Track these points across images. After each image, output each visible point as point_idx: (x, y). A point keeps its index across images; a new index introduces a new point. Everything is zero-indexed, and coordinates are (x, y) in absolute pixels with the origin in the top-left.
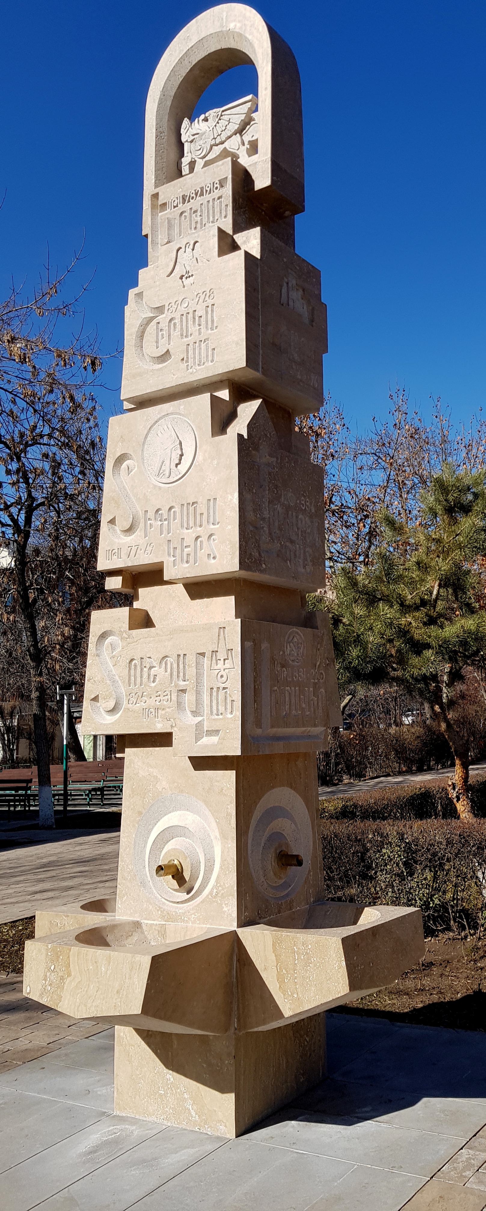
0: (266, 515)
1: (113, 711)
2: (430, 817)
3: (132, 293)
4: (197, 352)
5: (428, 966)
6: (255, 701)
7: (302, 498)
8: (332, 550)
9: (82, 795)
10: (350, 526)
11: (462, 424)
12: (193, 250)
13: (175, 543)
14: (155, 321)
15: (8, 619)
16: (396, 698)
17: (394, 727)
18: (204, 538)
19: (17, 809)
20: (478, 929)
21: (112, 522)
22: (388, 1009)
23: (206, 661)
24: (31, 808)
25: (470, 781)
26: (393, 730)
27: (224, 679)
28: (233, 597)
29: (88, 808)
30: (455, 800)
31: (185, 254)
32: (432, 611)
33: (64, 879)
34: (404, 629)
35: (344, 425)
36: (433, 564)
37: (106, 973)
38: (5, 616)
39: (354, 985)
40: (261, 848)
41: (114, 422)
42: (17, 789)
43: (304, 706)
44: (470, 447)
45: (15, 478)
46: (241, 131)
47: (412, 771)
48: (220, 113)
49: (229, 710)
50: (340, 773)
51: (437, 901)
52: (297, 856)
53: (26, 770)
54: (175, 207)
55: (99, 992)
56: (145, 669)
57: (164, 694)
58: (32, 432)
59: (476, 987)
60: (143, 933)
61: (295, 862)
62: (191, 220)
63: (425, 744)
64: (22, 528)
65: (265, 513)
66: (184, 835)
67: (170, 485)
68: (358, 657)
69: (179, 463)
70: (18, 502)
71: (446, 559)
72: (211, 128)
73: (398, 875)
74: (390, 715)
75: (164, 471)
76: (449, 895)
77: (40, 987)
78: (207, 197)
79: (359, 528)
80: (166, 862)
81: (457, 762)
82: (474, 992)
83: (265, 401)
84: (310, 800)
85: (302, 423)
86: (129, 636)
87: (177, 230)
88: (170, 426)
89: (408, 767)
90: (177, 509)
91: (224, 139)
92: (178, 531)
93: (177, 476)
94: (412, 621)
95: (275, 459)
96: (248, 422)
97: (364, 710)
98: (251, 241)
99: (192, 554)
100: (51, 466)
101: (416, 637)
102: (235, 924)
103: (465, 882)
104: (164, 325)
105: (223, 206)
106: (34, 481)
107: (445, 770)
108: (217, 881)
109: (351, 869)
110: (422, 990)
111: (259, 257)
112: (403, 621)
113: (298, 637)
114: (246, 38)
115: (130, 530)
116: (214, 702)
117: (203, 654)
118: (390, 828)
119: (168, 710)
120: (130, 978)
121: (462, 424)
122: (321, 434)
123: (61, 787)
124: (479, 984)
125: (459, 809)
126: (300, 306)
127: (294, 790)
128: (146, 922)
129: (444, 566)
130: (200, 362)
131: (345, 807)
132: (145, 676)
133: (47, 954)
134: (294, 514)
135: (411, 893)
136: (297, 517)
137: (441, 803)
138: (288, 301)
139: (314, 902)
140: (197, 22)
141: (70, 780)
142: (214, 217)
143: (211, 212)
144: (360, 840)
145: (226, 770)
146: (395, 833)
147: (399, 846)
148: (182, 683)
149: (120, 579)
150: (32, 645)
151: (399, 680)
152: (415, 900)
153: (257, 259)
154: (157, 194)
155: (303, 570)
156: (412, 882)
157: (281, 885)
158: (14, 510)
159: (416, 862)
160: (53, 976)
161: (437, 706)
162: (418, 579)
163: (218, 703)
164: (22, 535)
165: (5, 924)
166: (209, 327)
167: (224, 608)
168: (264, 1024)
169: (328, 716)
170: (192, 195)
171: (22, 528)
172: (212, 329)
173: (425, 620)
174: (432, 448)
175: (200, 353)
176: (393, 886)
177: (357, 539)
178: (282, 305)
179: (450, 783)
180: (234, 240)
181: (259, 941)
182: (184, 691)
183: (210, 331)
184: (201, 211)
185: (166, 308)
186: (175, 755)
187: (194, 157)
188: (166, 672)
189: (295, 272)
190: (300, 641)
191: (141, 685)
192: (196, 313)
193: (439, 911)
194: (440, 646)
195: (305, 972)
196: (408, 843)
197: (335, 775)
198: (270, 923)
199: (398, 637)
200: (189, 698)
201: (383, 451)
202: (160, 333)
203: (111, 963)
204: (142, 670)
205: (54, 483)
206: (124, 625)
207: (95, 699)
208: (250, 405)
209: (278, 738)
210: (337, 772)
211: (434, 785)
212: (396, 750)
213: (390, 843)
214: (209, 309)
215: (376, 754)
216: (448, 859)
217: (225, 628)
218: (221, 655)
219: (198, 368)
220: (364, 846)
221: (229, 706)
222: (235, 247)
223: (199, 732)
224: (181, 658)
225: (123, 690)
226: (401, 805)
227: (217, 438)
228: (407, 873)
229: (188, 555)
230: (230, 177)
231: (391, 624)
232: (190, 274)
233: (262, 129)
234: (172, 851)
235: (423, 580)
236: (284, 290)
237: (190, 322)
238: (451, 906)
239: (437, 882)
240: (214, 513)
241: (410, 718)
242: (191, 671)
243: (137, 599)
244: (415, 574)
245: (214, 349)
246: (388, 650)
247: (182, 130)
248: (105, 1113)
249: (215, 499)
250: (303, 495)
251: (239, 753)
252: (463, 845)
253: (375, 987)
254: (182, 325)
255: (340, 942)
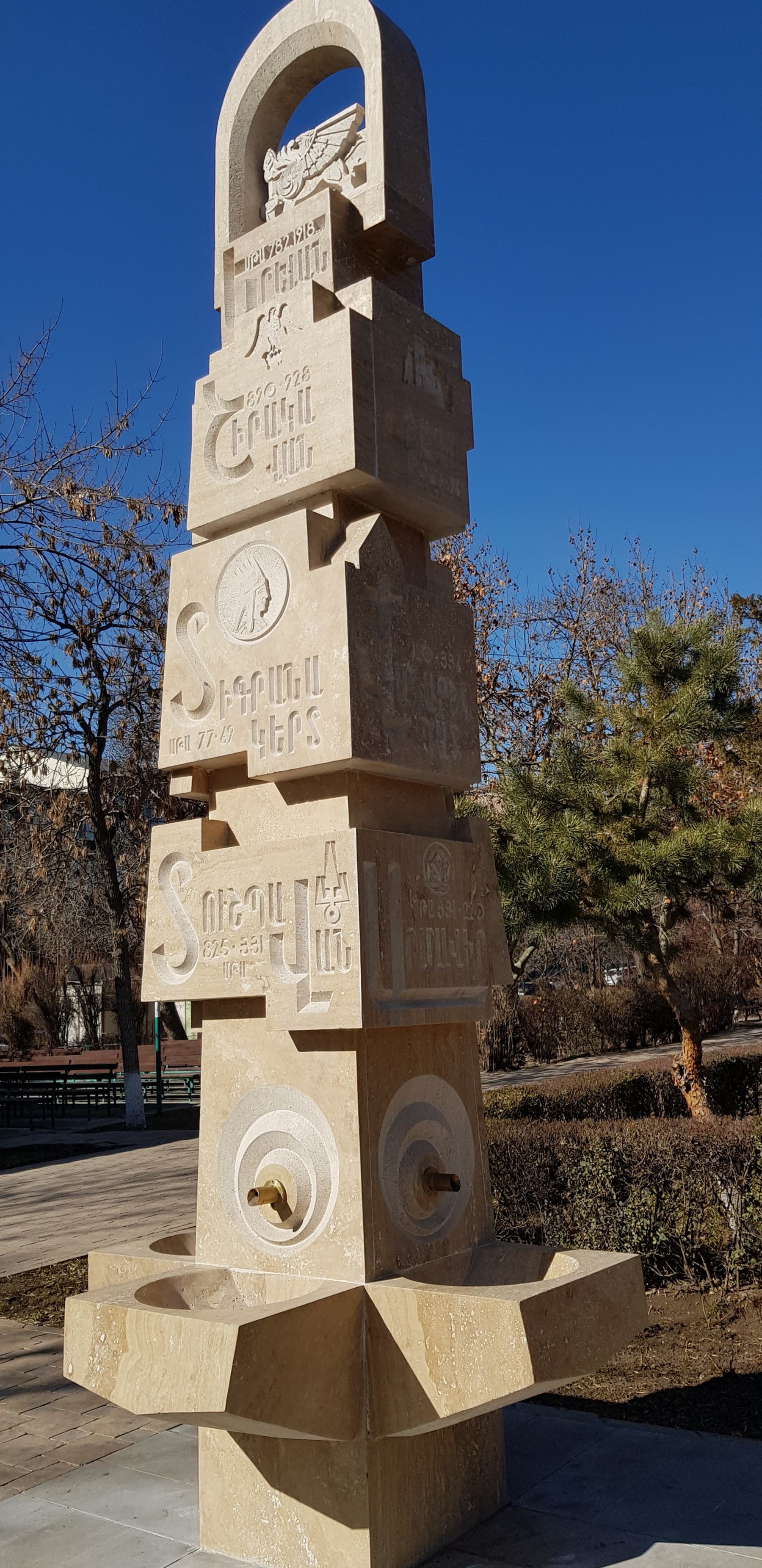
0: (390, 676)
1: (183, 967)
2: (648, 1115)
3: (200, 384)
4: (288, 455)
5: (652, 1331)
6: (381, 949)
7: (443, 653)
8: (500, 749)
9: (182, 1084)
10: (522, 716)
11: (670, 573)
12: (280, 316)
13: (263, 725)
14: (231, 419)
15: (80, 854)
16: (595, 950)
17: (593, 988)
18: (302, 715)
19: (99, 1103)
20: (724, 1277)
21: (177, 699)
22: (596, 1396)
23: (309, 891)
24: (118, 1102)
25: (704, 1062)
26: (592, 993)
27: (335, 917)
28: (346, 798)
29: (190, 1102)
30: (683, 1090)
31: (269, 324)
32: (640, 820)
33: (153, 1199)
34: (600, 848)
35: (510, 581)
36: (638, 753)
37: (176, 1348)
38: (76, 849)
39: (539, 1374)
40: (398, 1165)
41: (177, 560)
42: (99, 1077)
43: (454, 954)
44: (683, 603)
45: (85, 671)
46: (343, 155)
47: (619, 1048)
48: (313, 136)
49: (343, 963)
50: (521, 1052)
51: (662, 1237)
52: (451, 1177)
53: (112, 1051)
54: (255, 264)
55: (167, 1377)
56: (226, 906)
57: (253, 941)
58: (104, 611)
59: (725, 1364)
60: (233, 1286)
61: (448, 1185)
62: (277, 279)
63: (637, 1011)
64: (96, 735)
65: (388, 674)
66: (287, 1145)
67: (254, 642)
68: (537, 887)
69: (266, 611)
70: (91, 702)
71: (657, 746)
72: (303, 157)
73: (604, 1199)
74: (587, 973)
75: (245, 623)
76: (680, 1228)
77: (87, 1366)
78: (299, 245)
79: (535, 717)
80: (263, 1185)
81: (685, 1035)
82: (724, 1373)
83: (385, 519)
84: (468, 1091)
85: (439, 551)
86: (202, 859)
87: (259, 294)
88: (252, 560)
89: (615, 1043)
90: (264, 675)
91: (320, 168)
92: (266, 706)
93: (263, 628)
94: (609, 834)
95: (401, 597)
96: (359, 547)
97: (552, 967)
98: (360, 296)
99: (286, 738)
100: (130, 653)
101: (619, 857)
102: (363, 1276)
103: (703, 1208)
104: (242, 423)
105: (321, 254)
106: (108, 673)
107: (667, 1047)
108: (335, 1213)
109: (536, 1190)
110: (646, 1368)
111: (371, 318)
112: (599, 835)
113: (443, 854)
114: (346, 28)
115: (201, 710)
116: (323, 950)
117: (304, 882)
118: (592, 1131)
119: (257, 963)
120: (209, 1358)
121: (670, 573)
122: (478, 592)
123: (153, 1073)
124: (731, 1362)
125: (689, 1103)
126: (431, 383)
127: (445, 1078)
128: (237, 1270)
129: (655, 755)
130: (292, 468)
131: (526, 1101)
132: (226, 915)
133: (95, 1318)
134: (431, 675)
135: (623, 1224)
136: (436, 680)
137: (663, 1094)
138: (415, 376)
139: (480, 1243)
140: (280, 17)
141: (165, 1064)
142: (308, 271)
143: (304, 264)
144: (547, 1149)
145: (343, 1050)
146: (598, 1139)
147: (605, 1157)
148: (276, 925)
149: (189, 779)
150: (110, 888)
151: (598, 921)
152: (631, 1235)
153: (369, 320)
154: (232, 250)
155: (447, 757)
156: (625, 1209)
157: (429, 1218)
158: (85, 713)
159: (629, 1180)
160: (103, 1351)
161: (653, 956)
162: (617, 776)
163: (327, 953)
164: (96, 744)
165: (73, 1260)
166: (304, 418)
167: (333, 815)
168: (409, 1426)
169: (491, 969)
170: (277, 246)
171: (96, 735)
172: (308, 421)
173: (630, 832)
174: (631, 607)
175: (292, 456)
176: (598, 1215)
177: (534, 734)
178: (406, 382)
179: (676, 1066)
180: (336, 299)
181: (400, 1304)
182: (279, 936)
183: (305, 425)
184: (291, 265)
185: (246, 400)
186: (269, 1028)
187: (281, 197)
188: (254, 909)
189: (424, 339)
190: (446, 860)
191: (220, 929)
192: (286, 402)
193: (666, 1250)
194: (654, 869)
195: (468, 1351)
196: (617, 1153)
197: (513, 1056)
198: (414, 1276)
199: (592, 859)
200: (287, 945)
201: (563, 614)
202: (238, 435)
203: (183, 1335)
204: (221, 907)
205: (133, 674)
206: (195, 844)
207: (160, 950)
208: (364, 523)
209: (416, 1003)
210: (517, 1051)
211: (652, 1068)
212: (597, 1021)
213: (592, 1152)
214: (304, 395)
215: (568, 1025)
216: (676, 1175)
217: (334, 842)
218: (330, 883)
219: (289, 476)
220: (553, 1156)
221: (343, 957)
222: (337, 306)
223: (303, 995)
224: (275, 888)
225: (196, 936)
226: (606, 1097)
227: (316, 570)
228: (617, 1196)
229: (281, 739)
230: (328, 214)
231: (582, 840)
232: (276, 350)
233: (372, 150)
234: (269, 1169)
235: (625, 777)
236: (408, 363)
237: (278, 415)
238: (684, 1243)
239: (661, 1209)
240: (315, 677)
241: (615, 977)
242: (289, 907)
243: (214, 807)
244: (614, 769)
245: (311, 448)
246: (578, 877)
247: (265, 165)
248: (188, 1547)
249: (316, 657)
250: (443, 647)
251: (359, 1025)
252: (699, 1156)
253: (573, 1375)
254: (267, 421)
255: (518, 1307)
